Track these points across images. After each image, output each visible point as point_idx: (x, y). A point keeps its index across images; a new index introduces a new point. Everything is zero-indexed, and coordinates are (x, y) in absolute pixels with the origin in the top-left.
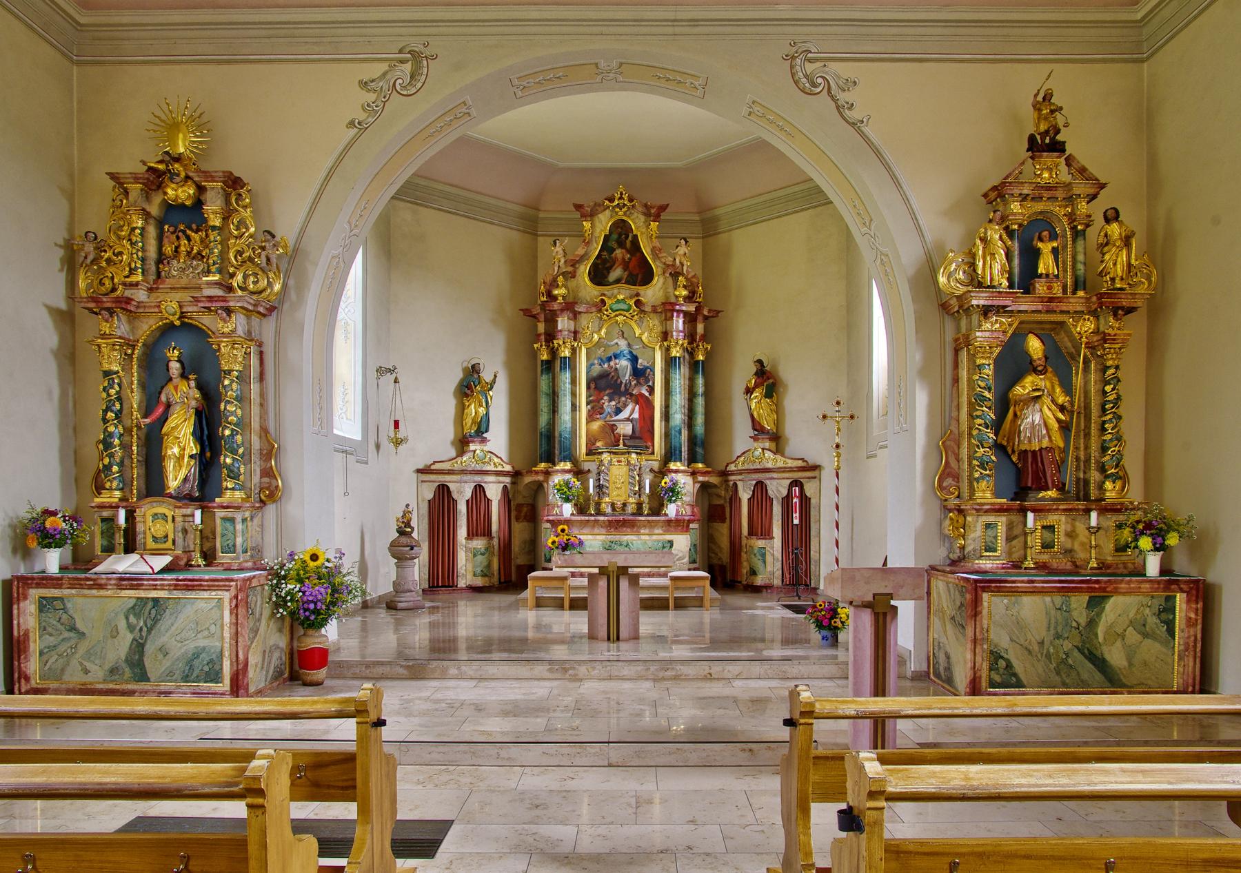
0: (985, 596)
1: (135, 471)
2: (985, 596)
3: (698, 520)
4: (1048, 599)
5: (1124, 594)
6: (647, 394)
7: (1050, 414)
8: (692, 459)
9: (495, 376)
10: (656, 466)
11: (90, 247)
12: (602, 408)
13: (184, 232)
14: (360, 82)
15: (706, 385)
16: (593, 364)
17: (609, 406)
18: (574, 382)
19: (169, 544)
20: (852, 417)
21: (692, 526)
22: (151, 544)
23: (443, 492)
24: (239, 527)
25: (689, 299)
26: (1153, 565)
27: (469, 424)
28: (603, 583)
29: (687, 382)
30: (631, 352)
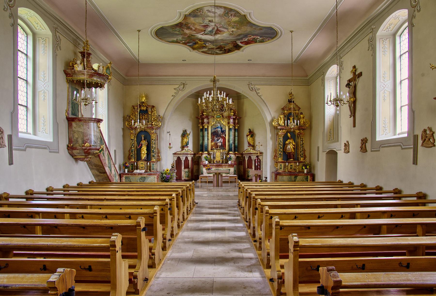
0: (278, 176)
1: (136, 156)
2: (278, 176)
3: (236, 165)
4: (288, 176)
5: (300, 176)
6: (224, 136)
7: (291, 146)
8: (235, 151)
9: (190, 132)
10: (226, 152)
11: (128, 118)
12: (214, 139)
13: (144, 115)
14: (174, 88)
15: (238, 134)
16: (212, 130)
17: (216, 139)
18: (208, 133)
19: (144, 168)
20: (262, 145)
21: (234, 166)
22: (140, 168)
23: (179, 159)
24: (155, 165)
25: (234, 115)
26: (305, 171)
27: (184, 143)
28: (216, 176)
29: (234, 133)
30: (221, 127)
